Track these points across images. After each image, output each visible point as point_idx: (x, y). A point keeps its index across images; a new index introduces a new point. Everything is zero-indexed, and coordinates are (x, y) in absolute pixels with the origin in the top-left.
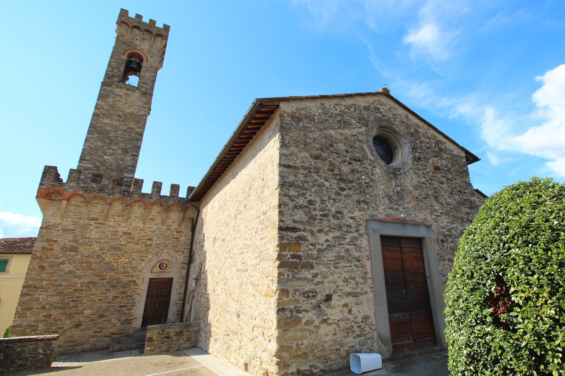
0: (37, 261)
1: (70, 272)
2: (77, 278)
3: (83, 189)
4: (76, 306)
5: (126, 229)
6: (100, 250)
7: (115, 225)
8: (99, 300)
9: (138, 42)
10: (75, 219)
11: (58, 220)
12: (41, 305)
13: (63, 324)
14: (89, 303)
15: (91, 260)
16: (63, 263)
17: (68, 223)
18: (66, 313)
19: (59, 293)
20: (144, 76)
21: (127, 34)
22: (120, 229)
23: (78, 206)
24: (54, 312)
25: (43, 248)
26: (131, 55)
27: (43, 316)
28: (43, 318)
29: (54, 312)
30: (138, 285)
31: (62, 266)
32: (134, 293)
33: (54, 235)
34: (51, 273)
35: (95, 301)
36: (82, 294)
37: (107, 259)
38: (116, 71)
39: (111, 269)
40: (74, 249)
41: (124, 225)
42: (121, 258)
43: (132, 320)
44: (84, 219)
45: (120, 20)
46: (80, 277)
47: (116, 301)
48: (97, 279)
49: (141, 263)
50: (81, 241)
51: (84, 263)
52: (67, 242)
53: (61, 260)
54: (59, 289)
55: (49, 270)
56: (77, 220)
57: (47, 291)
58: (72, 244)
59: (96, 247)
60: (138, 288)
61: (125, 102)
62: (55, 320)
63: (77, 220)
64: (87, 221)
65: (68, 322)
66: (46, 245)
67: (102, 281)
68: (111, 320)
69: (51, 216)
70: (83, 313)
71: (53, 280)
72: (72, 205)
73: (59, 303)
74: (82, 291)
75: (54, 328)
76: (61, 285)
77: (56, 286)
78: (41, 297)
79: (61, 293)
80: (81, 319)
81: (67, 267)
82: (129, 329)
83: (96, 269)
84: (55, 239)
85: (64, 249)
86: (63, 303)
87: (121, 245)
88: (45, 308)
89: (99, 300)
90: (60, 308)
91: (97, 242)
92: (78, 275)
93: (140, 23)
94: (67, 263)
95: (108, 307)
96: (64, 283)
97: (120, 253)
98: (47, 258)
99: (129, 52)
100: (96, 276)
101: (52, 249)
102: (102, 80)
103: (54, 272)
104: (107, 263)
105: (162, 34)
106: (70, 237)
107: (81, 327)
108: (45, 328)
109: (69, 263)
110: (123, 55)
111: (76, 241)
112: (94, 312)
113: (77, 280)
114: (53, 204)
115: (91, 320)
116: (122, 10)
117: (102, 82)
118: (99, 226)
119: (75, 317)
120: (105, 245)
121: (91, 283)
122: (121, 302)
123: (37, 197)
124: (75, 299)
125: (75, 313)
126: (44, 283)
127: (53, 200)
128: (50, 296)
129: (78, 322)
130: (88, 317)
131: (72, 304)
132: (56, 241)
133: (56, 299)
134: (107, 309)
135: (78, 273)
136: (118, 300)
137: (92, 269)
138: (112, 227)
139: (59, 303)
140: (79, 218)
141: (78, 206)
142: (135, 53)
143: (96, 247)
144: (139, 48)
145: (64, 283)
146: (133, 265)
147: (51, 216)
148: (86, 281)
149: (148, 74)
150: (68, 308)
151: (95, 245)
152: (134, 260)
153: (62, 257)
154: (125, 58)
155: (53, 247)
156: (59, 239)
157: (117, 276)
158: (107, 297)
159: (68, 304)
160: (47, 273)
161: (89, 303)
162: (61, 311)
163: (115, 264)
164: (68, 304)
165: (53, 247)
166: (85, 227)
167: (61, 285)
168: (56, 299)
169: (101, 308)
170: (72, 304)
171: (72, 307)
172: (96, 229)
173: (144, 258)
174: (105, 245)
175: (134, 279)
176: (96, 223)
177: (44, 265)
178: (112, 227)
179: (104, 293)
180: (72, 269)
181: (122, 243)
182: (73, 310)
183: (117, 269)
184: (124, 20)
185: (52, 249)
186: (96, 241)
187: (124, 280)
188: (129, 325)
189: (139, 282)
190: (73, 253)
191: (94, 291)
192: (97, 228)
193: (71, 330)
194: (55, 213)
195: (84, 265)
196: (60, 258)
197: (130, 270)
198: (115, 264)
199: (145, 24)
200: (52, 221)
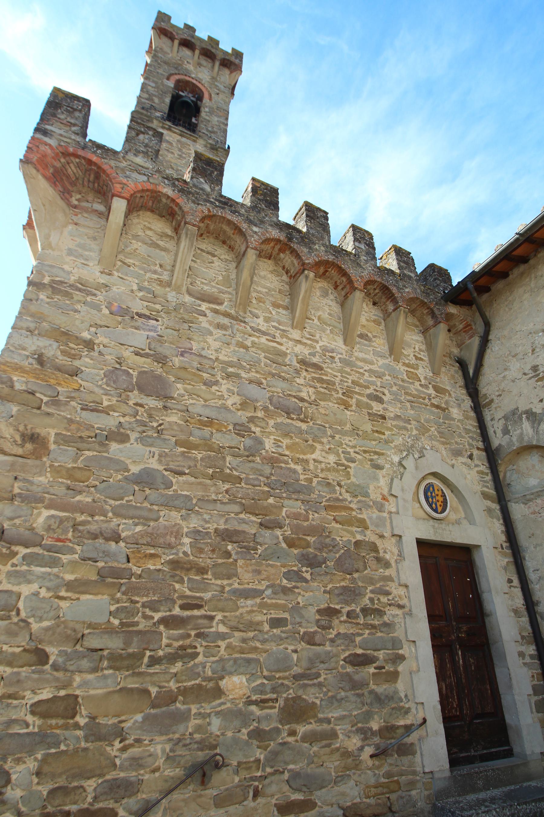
0: (14, 409)
1: (145, 479)
2: (178, 509)
3: (174, 185)
4: (184, 654)
5: (306, 351)
6: (244, 405)
7: (272, 331)
8: (276, 623)
9: (191, 67)
10: (150, 280)
11: (93, 273)
12: (23, 640)
13: (136, 763)
14: (236, 639)
15: (219, 439)
16: (121, 437)
17: (125, 288)
18: (146, 692)
19: (109, 578)
20: (209, 121)
21: (172, 51)
22: (287, 346)
23: (157, 246)
24: (91, 686)
25: (41, 360)
26: (181, 85)
27: (36, 709)
28: (35, 723)
29: (91, 686)
30: (387, 565)
31: (114, 446)
32: (384, 599)
33: (81, 320)
34: (70, 474)
35: (252, 626)
36: (204, 586)
37: (269, 444)
38: (156, 100)
39: (291, 487)
40: (153, 386)
41: (296, 334)
42: (313, 449)
43: (408, 729)
44: (178, 289)
45: (159, 25)
46: (188, 508)
47: (332, 634)
48: (250, 524)
49: (375, 478)
50: (177, 361)
51: (196, 447)
52: (127, 353)
53: (109, 422)
54: (107, 554)
55: (63, 456)
56: (158, 290)
57: (54, 563)
58: (146, 364)
59: (227, 394)
60: (390, 579)
61: (180, 156)
62: (95, 733)
63: (158, 290)
64: (188, 299)
65: (159, 747)
66: (52, 349)
67: (267, 533)
68: (334, 735)
69: (70, 252)
70: (218, 692)
71: (81, 509)
72: (136, 237)
73: (109, 630)
74: (202, 571)
75: (91, 785)
76: (117, 538)
77: (95, 536)
78: (26, 590)
79: (116, 573)
80: (216, 725)
81: (136, 456)
82: (412, 784)
83: (239, 480)
84: (86, 335)
85: (116, 373)
86: (127, 630)
87: (302, 400)
88: (42, 657)
89: (276, 623)
90: (117, 661)
91: (229, 376)
92: (177, 496)
93: (193, 36)
94: (133, 436)
95: (311, 661)
96: (129, 529)
97: (304, 426)
98: (55, 402)
99: (177, 77)
100: (245, 509)
101: (75, 373)
102: (133, 109)
103: (87, 468)
104: (272, 461)
105: (232, 63)
106: (139, 338)
107: (225, 780)
108: (44, 790)
109: (141, 440)
110: (168, 79)
111: (162, 360)
112: (260, 689)
113: (175, 516)
114: (75, 218)
115: (258, 735)
116: (159, 12)
117: (133, 113)
118: (226, 321)
119: (185, 717)
120: (253, 391)
121: (228, 535)
122: (349, 638)
123: (25, 162)
124: (177, 611)
125: (184, 692)
126: (42, 517)
127: (75, 207)
128: (70, 586)
129: (202, 745)
130: (244, 717)
131: (168, 640)
132: (89, 345)
133: (96, 606)
134: (306, 676)
135: (180, 485)
136: (340, 627)
137: (227, 479)
138: (264, 333)
139: (109, 630)
140: (160, 282)
141: (157, 246)
142: (187, 82)
143: (227, 394)
144: (193, 76)
145: (129, 529)
146: (353, 479)
147: (70, 252)
148: (212, 527)
149: (216, 119)
150: (154, 661)
151: (225, 386)
152: (353, 461)
153: (111, 408)
154: (171, 84)
155: (77, 363)
156: (101, 339)
157: (315, 518)
158: (296, 609)
159: (149, 636)
160: (56, 471)
161: (236, 639)
162: (124, 679)
163: (299, 468)
164: (149, 636)
165: (77, 363)
166: (186, 319)
167: (117, 538)
168: (96, 606)
169: (283, 663)
170: (168, 640)
171: (172, 658)
172: (220, 332)
173: (381, 461)
174: (253, 391)
175: (370, 536)
176: (216, 312)
177: (42, 432)
178: (264, 333)
179: (285, 591)
180: (154, 464)
181: (304, 395)
182: (169, 678)
183: (309, 489)
184: (163, 27)
185: (75, 373)
186: (223, 370)
187: (344, 536)
188: (405, 760)
189: (388, 549)
190: (152, 402)
191: (246, 577)
192: (219, 326)
193: (176, 796)
194: (83, 246)
195: (198, 455)
196: (106, 412)
197: (347, 496)
198: (299, 468)
199: (199, 39)
200: (74, 271)
